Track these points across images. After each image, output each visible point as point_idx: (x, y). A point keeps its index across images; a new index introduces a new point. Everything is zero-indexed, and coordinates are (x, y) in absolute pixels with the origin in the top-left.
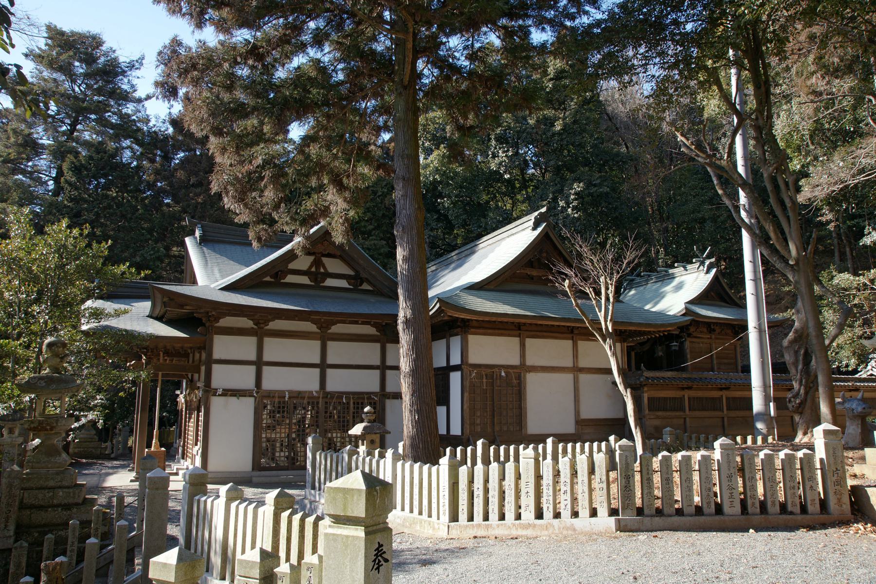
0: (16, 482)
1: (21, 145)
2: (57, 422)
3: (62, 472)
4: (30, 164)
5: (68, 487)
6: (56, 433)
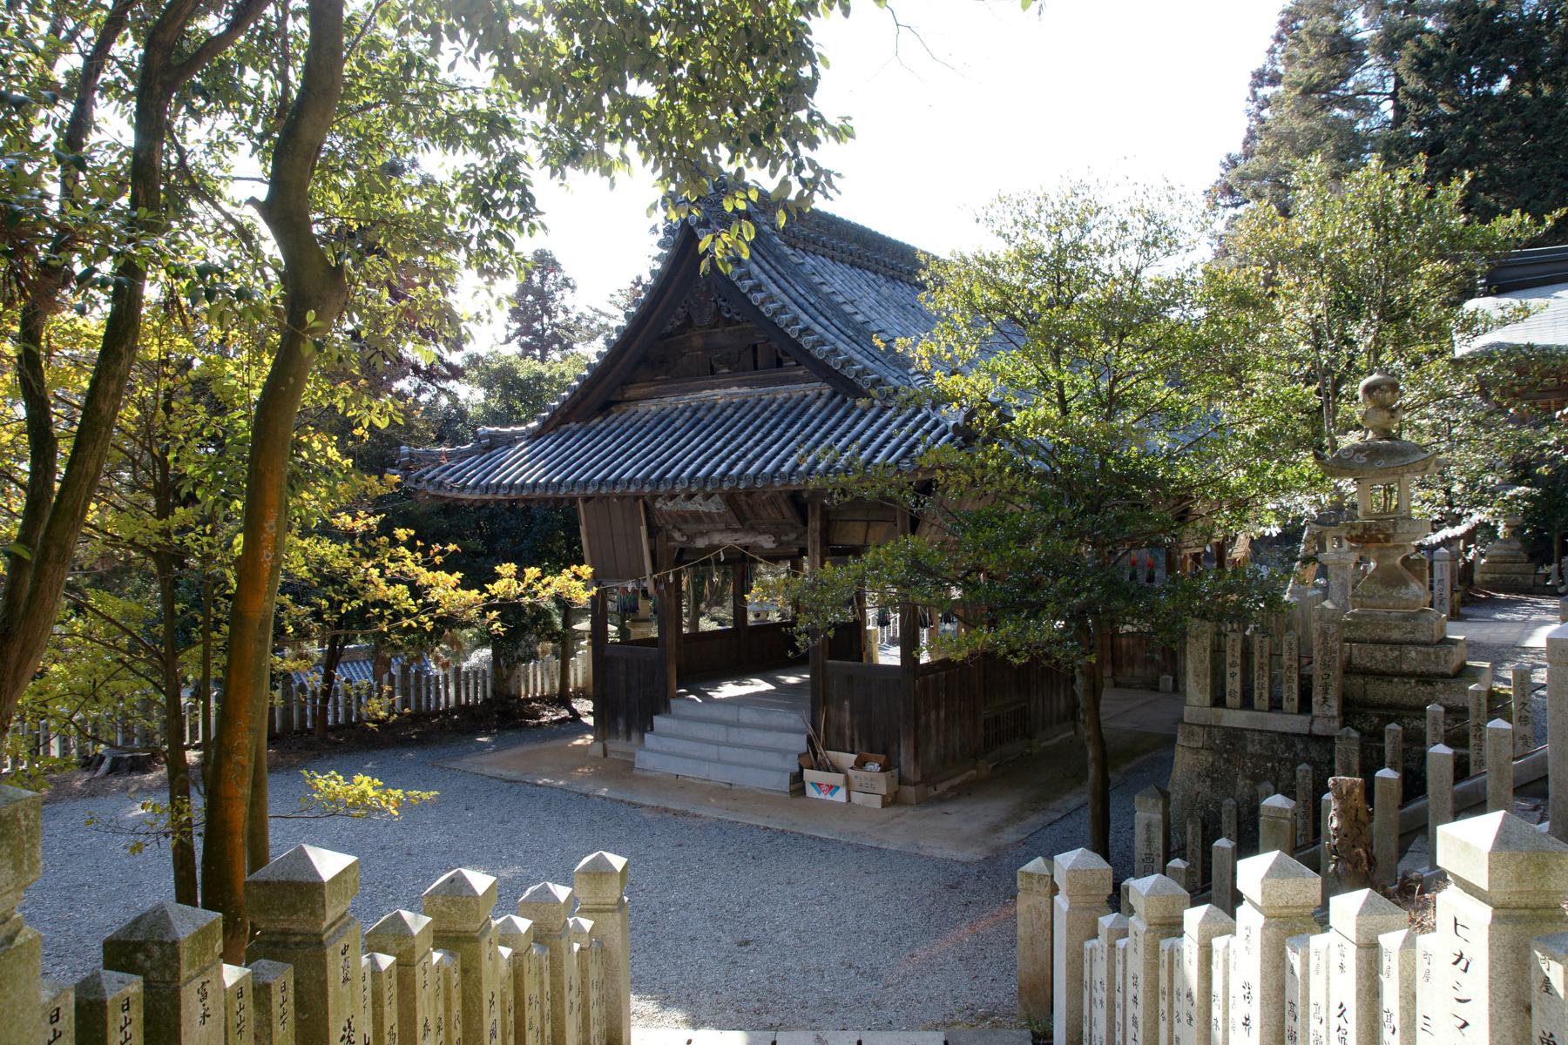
0: (1333, 629)
1: (1329, 55)
2: (1395, 525)
3: (1414, 617)
4: (1351, 83)
5: (1426, 644)
6: (1397, 547)
